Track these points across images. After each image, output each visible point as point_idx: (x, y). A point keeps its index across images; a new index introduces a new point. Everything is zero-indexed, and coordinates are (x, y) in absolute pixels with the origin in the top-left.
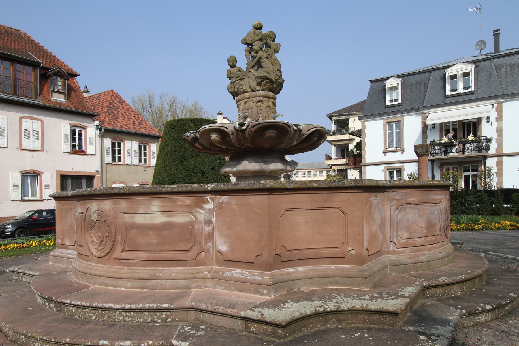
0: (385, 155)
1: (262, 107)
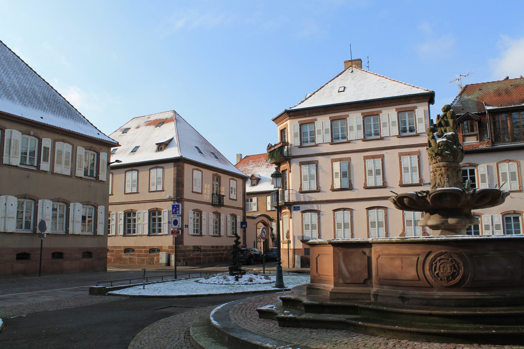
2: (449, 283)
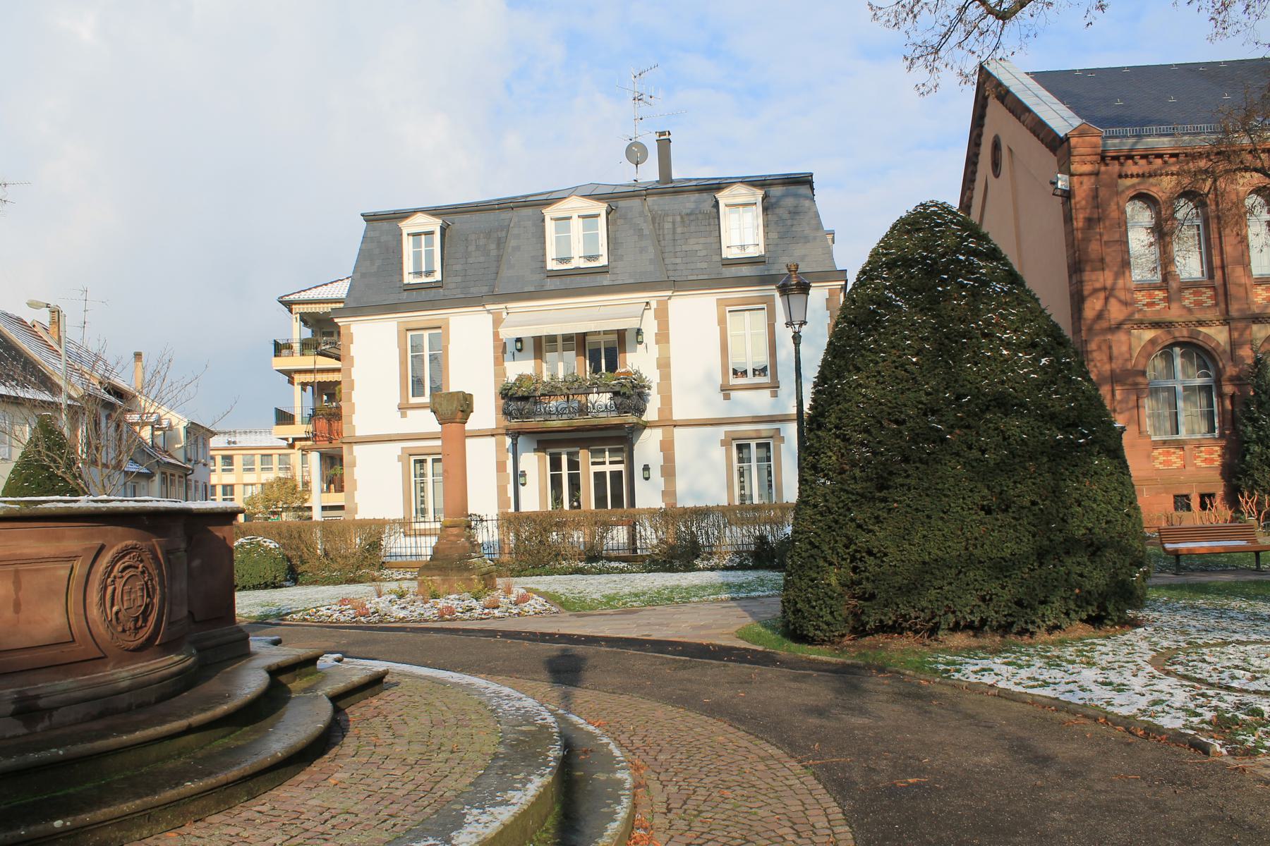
0: (404, 415)
2: (137, 637)
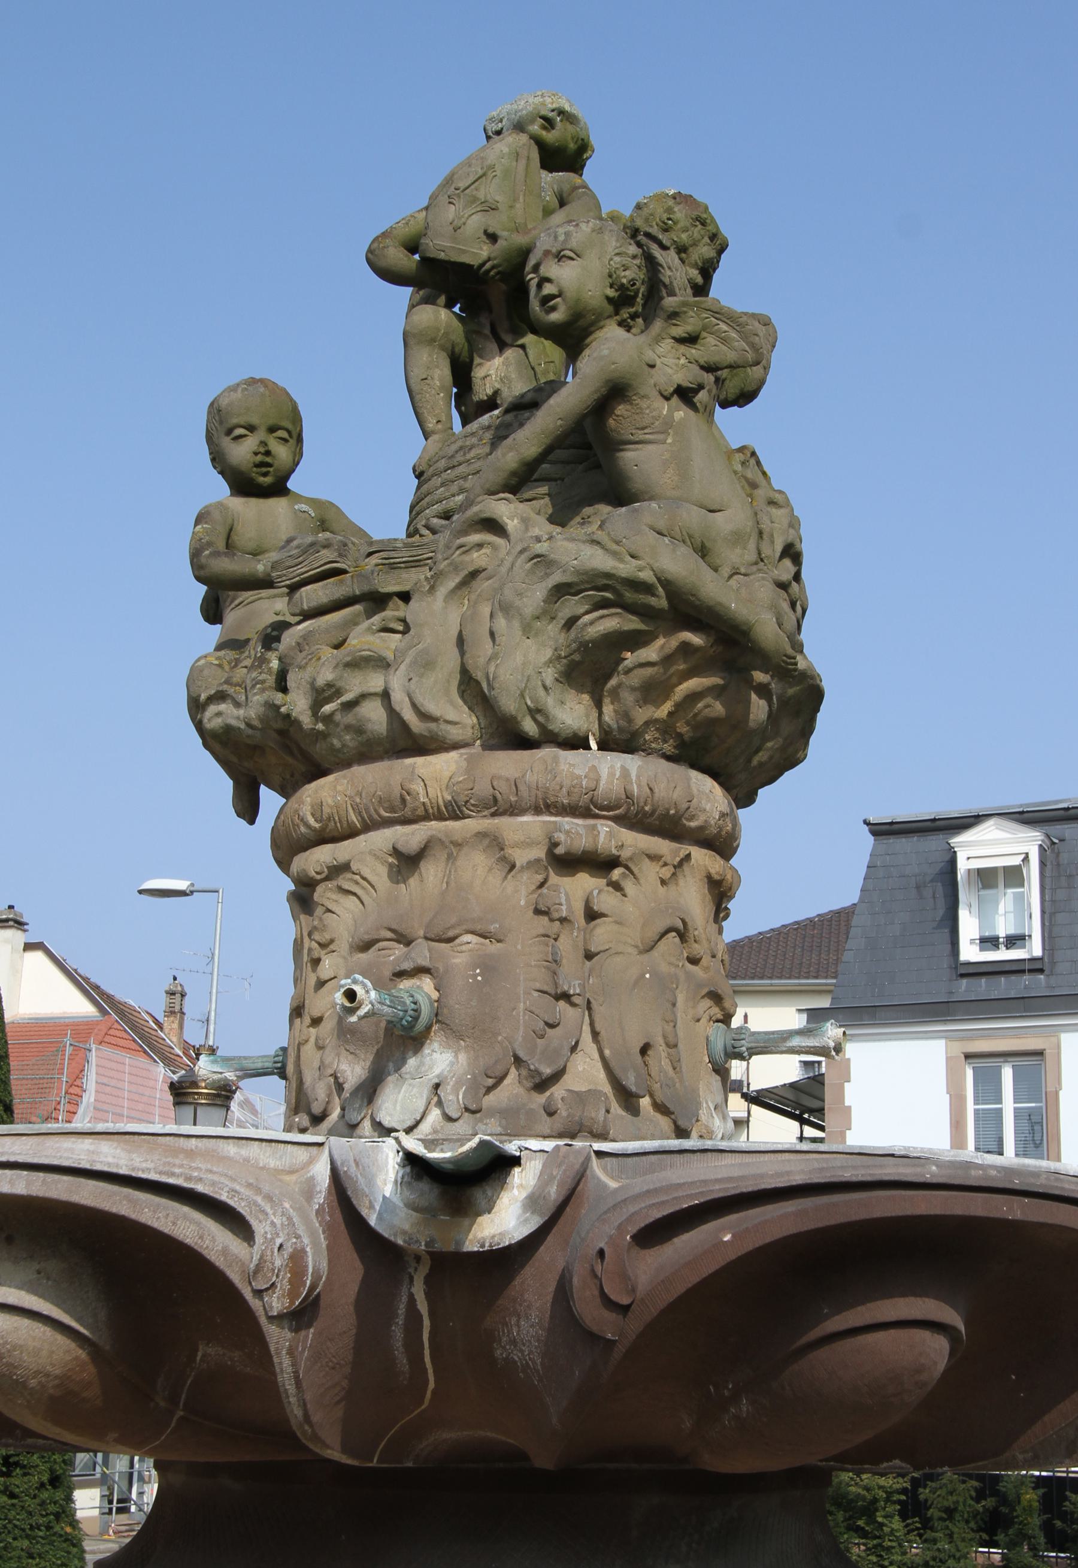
1: (602, 934)
